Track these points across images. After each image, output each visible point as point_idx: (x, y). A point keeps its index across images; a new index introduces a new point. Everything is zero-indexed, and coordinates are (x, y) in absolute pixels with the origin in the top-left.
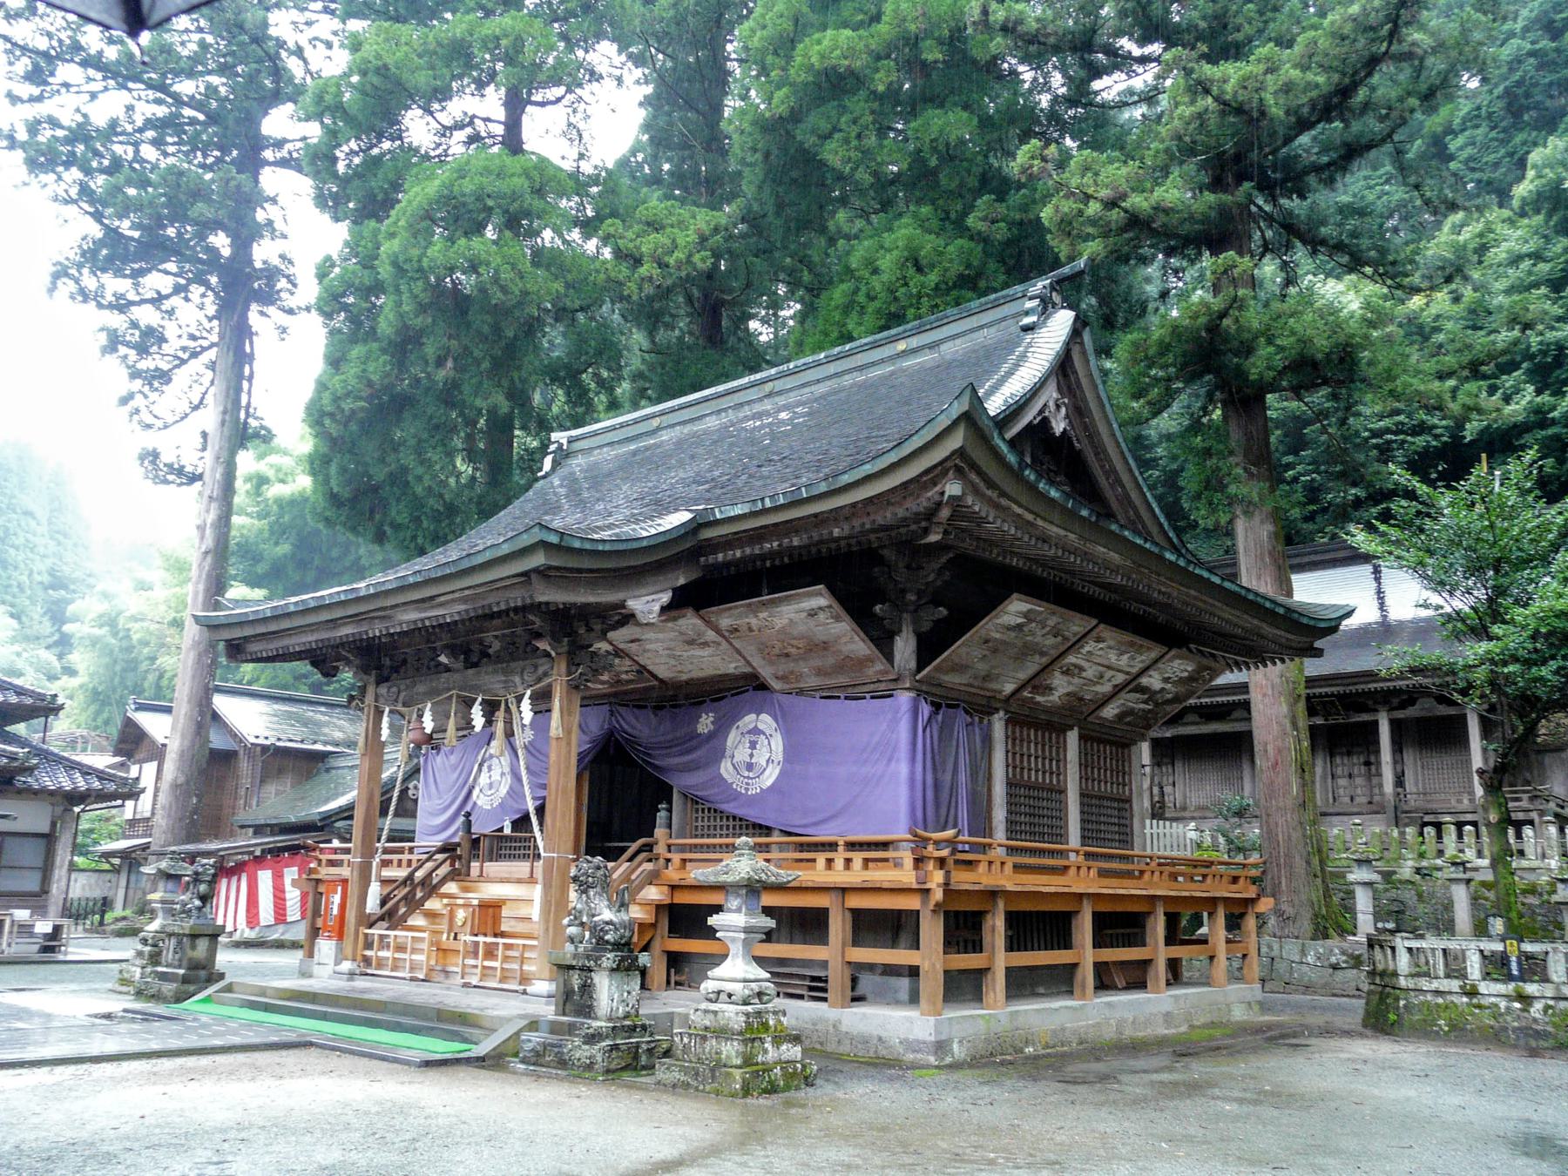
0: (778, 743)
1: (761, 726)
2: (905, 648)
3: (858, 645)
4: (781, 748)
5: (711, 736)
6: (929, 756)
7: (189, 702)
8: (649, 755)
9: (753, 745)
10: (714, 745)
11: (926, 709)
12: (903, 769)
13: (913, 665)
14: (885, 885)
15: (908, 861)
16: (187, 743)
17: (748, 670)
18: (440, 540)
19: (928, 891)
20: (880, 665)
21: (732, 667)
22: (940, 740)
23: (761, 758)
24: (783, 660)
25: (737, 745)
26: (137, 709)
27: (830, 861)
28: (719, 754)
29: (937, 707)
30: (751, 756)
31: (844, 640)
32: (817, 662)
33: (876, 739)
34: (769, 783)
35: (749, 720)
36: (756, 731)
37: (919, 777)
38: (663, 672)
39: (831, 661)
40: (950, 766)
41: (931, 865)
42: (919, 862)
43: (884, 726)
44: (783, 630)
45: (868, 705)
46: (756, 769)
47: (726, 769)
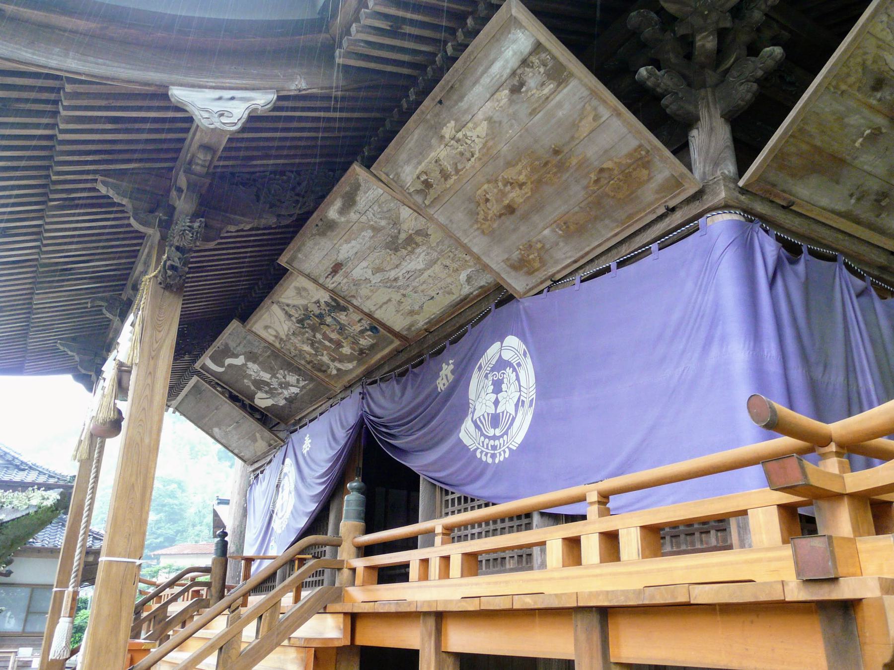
0: (528, 374)
1: (507, 355)
2: (710, 139)
3: (616, 132)
4: (532, 380)
5: (452, 388)
6: (789, 332)
7: (239, 494)
8: (393, 436)
9: (498, 387)
10: (455, 402)
11: (768, 248)
12: (738, 354)
13: (730, 168)
14: (702, 596)
15: (765, 523)
16: (237, 523)
17: (484, 280)
18: (143, 225)
19: (848, 608)
20: (666, 164)
21: (462, 284)
22: (807, 309)
23: (507, 406)
24: (509, 221)
25: (481, 398)
26: (219, 503)
27: (573, 543)
28: (463, 409)
29: (791, 250)
30: (496, 403)
31: (586, 125)
32: (557, 209)
33: (676, 316)
34: (519, 439)
35: (492, 352)
36: (502, 364)
37: (773, 366)
38: (399, 323)
39: (577, 193)
40: (838, 361)
41: (841, 522)
42: (799, 522)
43: (689, 285)
44: (488, 155)
45: (657, 259)
46: (503, 422)
47: (467, 434)
